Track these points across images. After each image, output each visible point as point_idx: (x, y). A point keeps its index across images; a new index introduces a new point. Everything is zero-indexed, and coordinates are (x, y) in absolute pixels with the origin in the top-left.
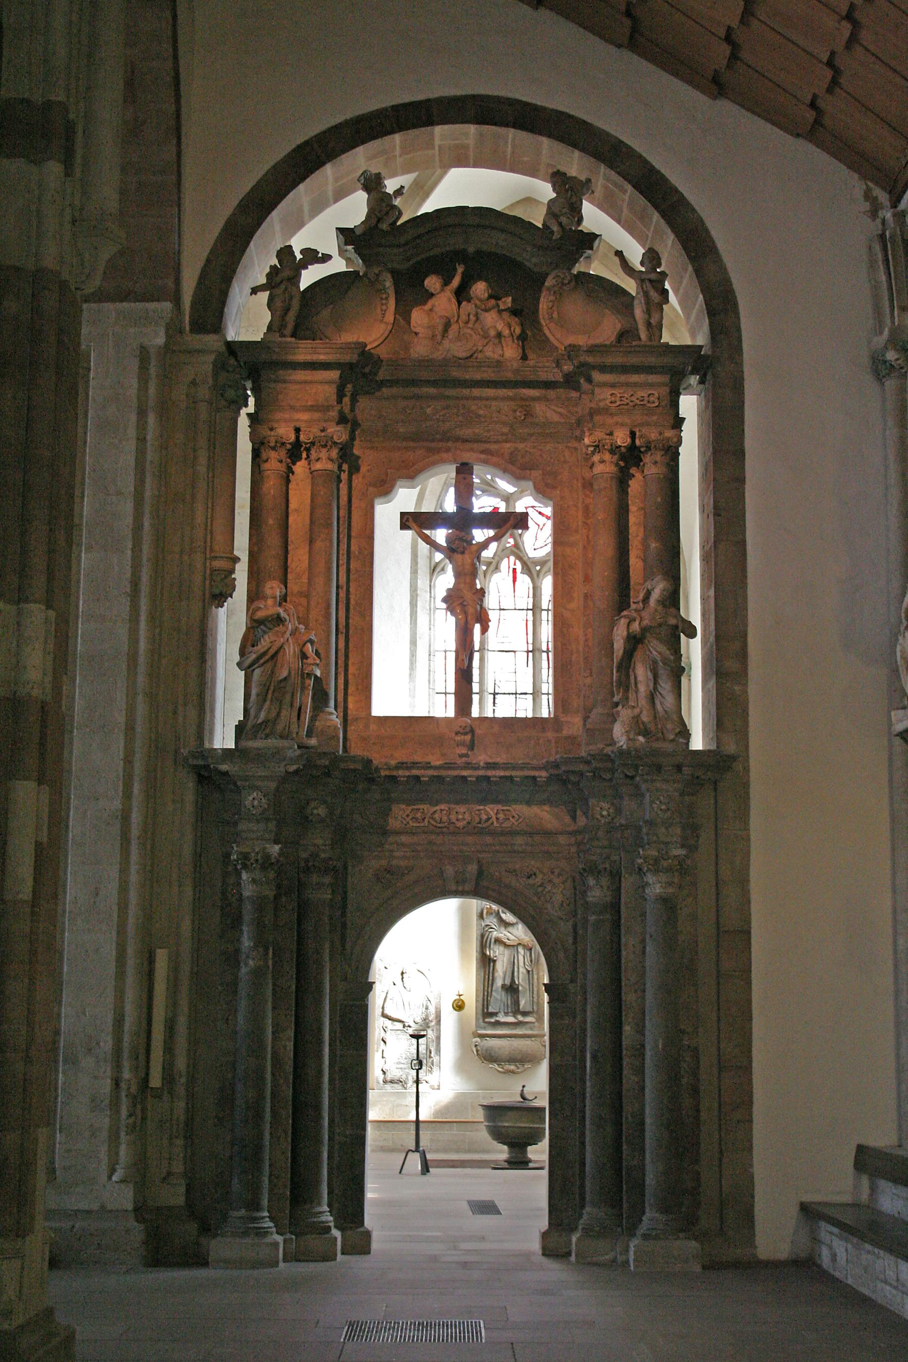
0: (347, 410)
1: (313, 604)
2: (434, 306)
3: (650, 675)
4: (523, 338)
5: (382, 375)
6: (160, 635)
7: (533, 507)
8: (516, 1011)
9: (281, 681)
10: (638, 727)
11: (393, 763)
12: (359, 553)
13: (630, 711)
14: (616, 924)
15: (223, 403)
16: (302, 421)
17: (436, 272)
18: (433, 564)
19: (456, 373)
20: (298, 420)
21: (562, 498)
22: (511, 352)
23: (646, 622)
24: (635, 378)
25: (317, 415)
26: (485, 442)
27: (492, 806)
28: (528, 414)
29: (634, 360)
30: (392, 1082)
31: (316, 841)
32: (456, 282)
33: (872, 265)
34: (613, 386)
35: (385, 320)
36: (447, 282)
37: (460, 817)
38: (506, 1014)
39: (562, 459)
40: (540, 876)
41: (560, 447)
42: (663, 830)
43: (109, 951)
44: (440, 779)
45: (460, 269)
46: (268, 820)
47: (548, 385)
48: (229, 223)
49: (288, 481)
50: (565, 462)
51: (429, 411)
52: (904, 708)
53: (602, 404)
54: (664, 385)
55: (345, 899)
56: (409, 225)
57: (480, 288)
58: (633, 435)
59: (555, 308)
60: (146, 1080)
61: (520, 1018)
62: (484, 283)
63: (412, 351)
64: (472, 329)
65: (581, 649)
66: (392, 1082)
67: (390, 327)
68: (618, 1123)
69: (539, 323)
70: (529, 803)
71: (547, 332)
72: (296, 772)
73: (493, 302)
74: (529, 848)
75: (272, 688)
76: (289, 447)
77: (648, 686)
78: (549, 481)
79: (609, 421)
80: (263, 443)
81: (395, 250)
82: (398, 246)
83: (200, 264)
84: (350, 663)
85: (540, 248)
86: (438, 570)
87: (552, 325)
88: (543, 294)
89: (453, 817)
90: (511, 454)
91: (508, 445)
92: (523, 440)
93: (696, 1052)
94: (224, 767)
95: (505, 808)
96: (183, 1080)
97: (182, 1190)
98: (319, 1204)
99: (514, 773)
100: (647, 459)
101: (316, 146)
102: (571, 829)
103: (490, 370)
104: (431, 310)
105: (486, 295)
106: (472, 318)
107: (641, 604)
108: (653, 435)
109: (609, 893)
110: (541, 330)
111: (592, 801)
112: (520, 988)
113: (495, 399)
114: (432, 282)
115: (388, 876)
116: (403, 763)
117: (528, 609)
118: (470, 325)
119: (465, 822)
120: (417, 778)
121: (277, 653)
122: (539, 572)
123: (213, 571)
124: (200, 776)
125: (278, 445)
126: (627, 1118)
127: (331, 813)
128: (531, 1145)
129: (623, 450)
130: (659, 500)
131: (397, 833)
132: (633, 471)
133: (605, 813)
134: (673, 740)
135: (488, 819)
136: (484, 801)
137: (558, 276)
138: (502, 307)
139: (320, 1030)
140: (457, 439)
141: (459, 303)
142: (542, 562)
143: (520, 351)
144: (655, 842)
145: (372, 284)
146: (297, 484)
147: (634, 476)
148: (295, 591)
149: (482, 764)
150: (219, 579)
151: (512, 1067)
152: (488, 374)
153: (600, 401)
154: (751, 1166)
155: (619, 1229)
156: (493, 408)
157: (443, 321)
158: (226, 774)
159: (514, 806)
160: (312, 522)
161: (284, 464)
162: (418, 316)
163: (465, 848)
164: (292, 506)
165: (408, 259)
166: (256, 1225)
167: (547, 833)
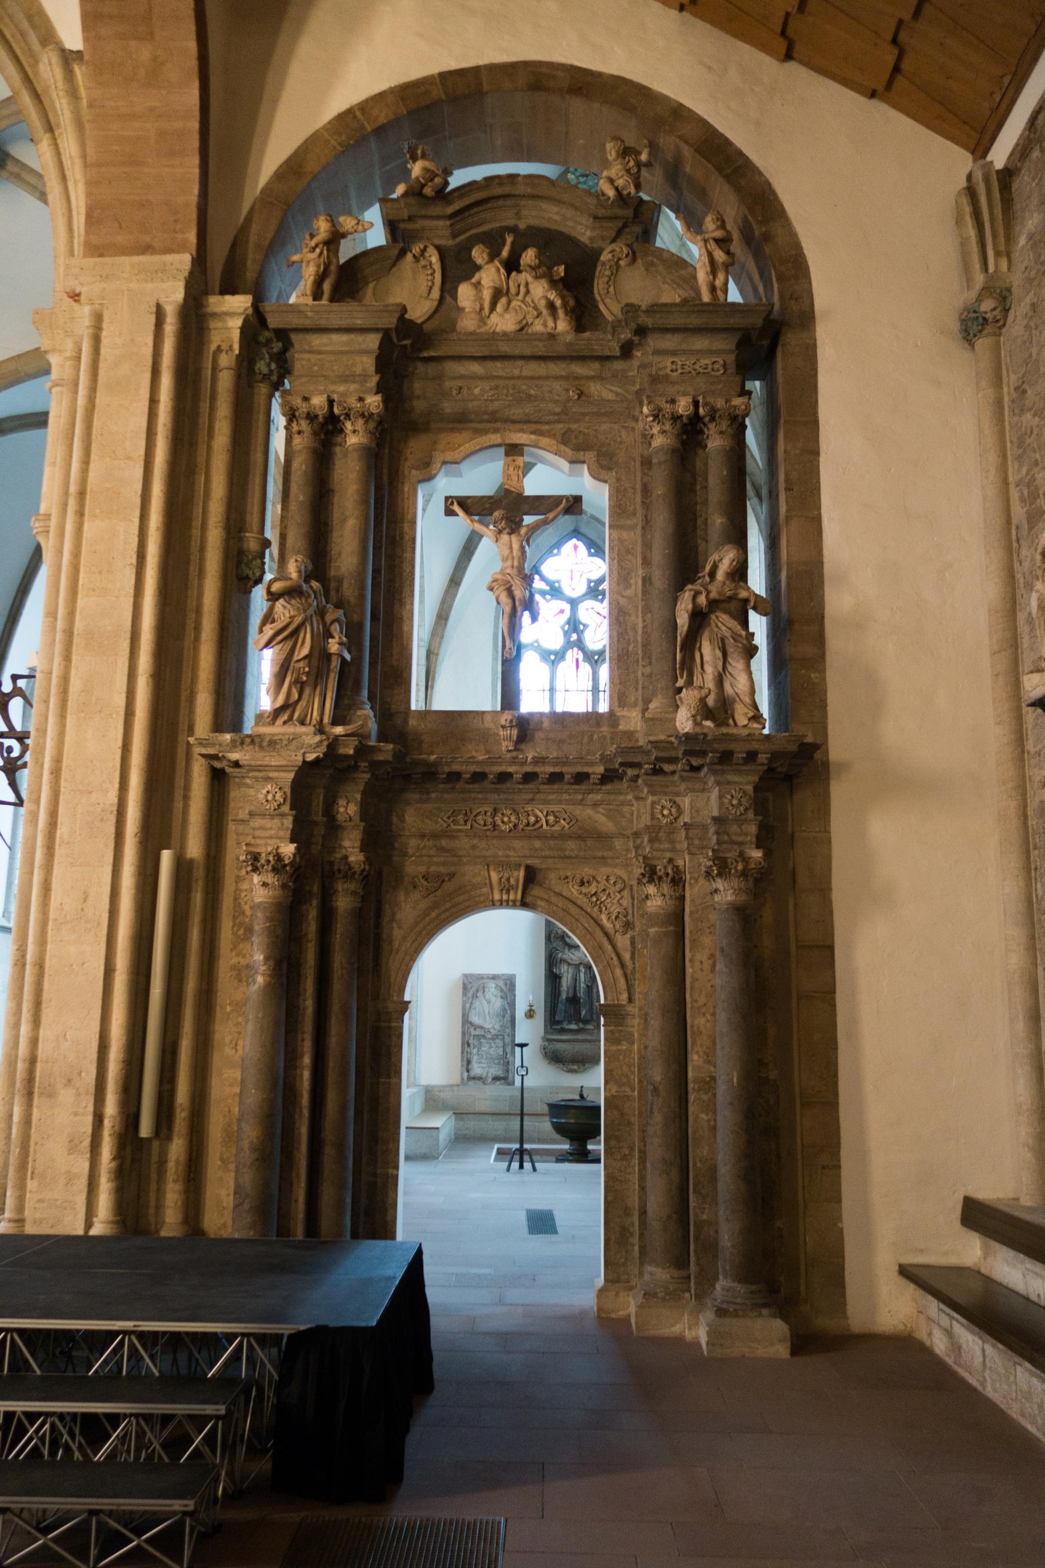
3: (719, 654)
8: (579, 1020)
10: (705, 711)
13: (696, 692)
14: (680, 935)
21: (618, 480)
22: (563, 325)
23: (713, 595)
26: (536, 422)
27: (541, 807)
30: (474, 1078)
33: (959, 222)
34: (674, 353)
36: (494, 255)
39: (619, 439)
40: (594, 884)
41: (616, 427)
46: (282, 815)
51: (477, 391)
52: (1039, 671)
53: (662, 373)
54: (730, 351)
58: (696, 404)
59: (611, 283)
61: (581, 1025)
65: (639, 639)
66: (474, 1078)
68: (684, 1170)
77: (716, 667)
78: (604, 463)
79: (671, 390)
90: (564, 434)
91: (561, 426)
92: (577, 421)
106: (523, 290)
122: (596, 662)
126: (695, 1164)
129: (685, 420)
133: (666, 812)
134: (745, 726)
135: (537, 822)
140: (507, 420)
141: (509, 274)
142: (601, 653)
151: (575, 1067)
152: (540, 348)
153: (661, 369)
154: (840, 1218)
155: (687, 1295)
162: (465, 292)
163: (511, 853)
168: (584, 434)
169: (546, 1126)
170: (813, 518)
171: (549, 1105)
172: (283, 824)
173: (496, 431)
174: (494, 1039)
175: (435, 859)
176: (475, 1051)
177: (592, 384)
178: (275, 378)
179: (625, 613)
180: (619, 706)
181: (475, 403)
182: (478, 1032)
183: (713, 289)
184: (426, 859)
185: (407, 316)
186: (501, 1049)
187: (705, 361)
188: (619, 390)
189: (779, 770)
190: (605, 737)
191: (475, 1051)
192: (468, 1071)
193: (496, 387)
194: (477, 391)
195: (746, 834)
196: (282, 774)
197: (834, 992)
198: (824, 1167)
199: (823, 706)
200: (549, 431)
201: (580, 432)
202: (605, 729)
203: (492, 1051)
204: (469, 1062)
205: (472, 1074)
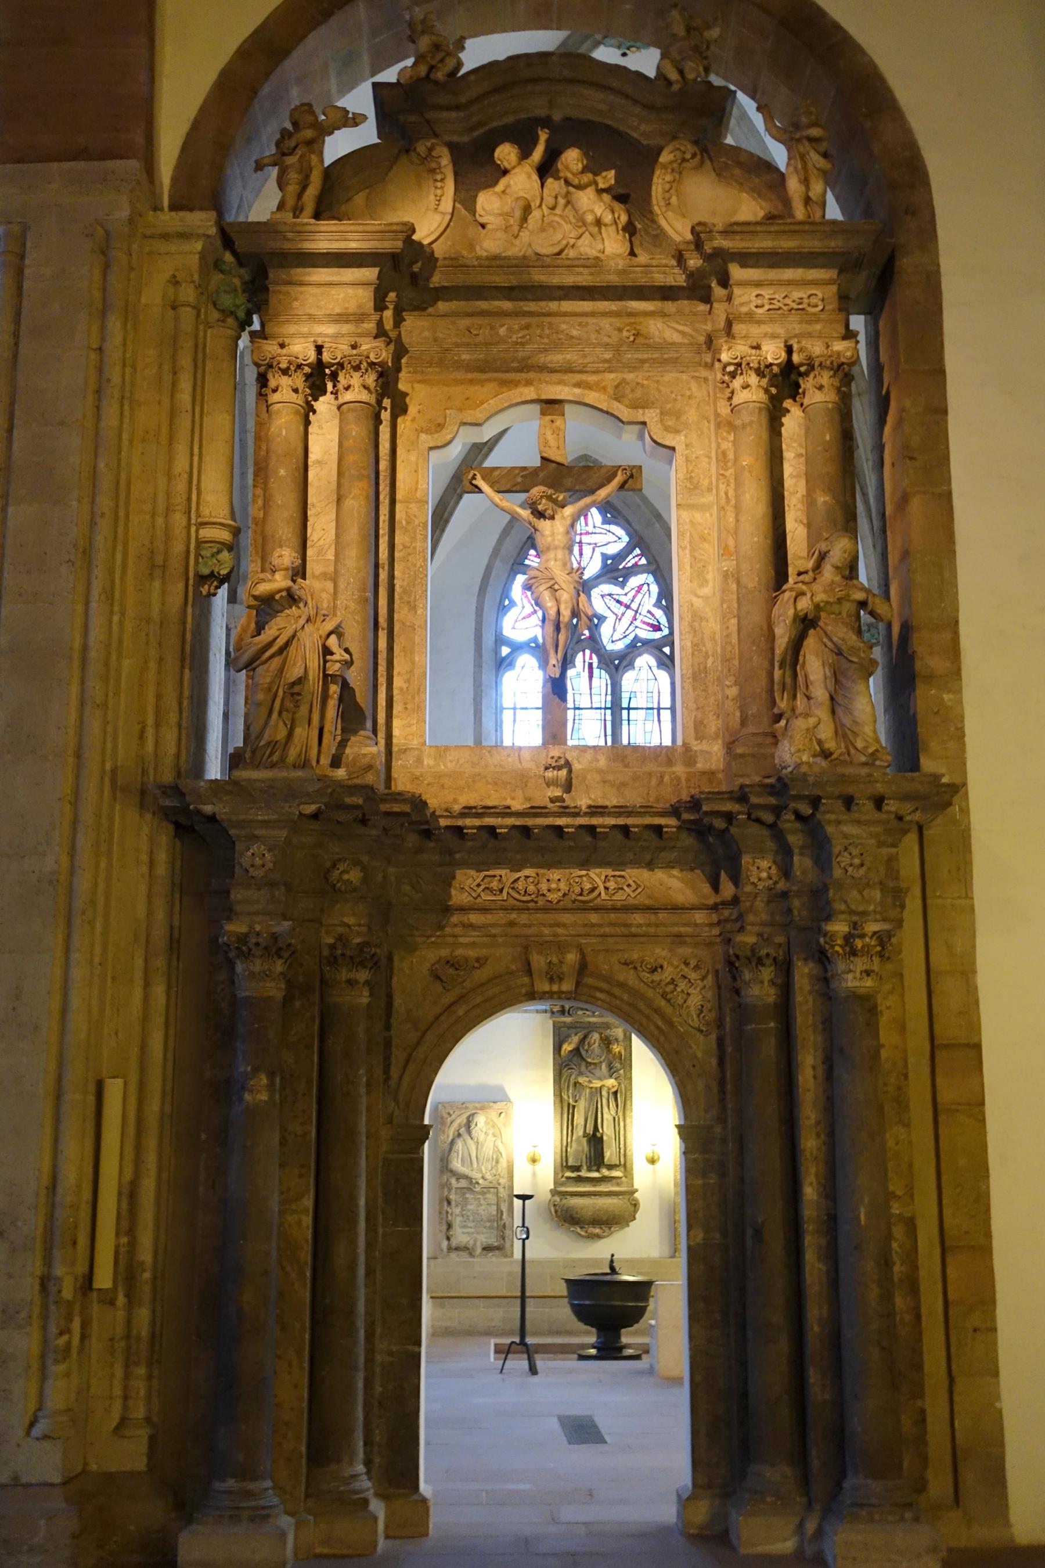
0: (389, 325)
1: (342, 585)
2: (508, 186)
4: (630, 229)
5: (437, 280)
6: (121, 623)
7: (610, 595)
9: (293, 684)
11: (457, 808)
12: (408, 523)
15: (215, 315)
16: (326, 336)
17: (513, 141)
18: (499, 660)
19: (539, 277)
20: (320, 335)
22: (612, 245)
23: (821, 597)
24: (789, 274)
25: (346, 328)
26: (580, 372)
27: (598, 870)
29: (787, 244)
30: (457, 1249)
31: (346, 920)
34: (759, 284)
35: (441, 208)
36: (525, 154)
37: (554, 886)
38: (589, 1170)
39: (688, 393)
40: (670, 969)
41: (684, 377)
42: (855, 893)
44: (525, 830)
45: (543, 136)
47: (667, 293)
49: (307, 423)
51: (502, 331)
53: (744, 309)
55: (389, 1006)
56: (472, 77)
57: (572, 158)
58: (789, 350)
59: (673, 191)
60: (89, 1277)
62: (577, 150)
63: (478, 248)
64: (561, 216)
66: (457, 1249)
67: (448, 217)
69: (651, 212)
70: (650, 865)
71: (663, 223)
72: (315, 816)
73: (588, 177)
74: (652, 930)
75: (281, 693)
76: (307, 370)
78: (670, 423)
79: (756, 331)
80: (270, 366)
81: (454, 114)
82: (457, 108)
83: (184, 128)
84: (395, 673)
86: (505, 664)
87: (670, 214)
88: (658, 172)
89: (544, 887)
90: (617, 387)
91: (612, 376)
92: (633, 369)
93: (911, 1225)
94: (208, 809)
95: (617, 873)
96: (147, 1275)
97: (143, 1447)
98: (351, 1462)
99: (630, 821)
100: (807, 384)
102: (710, 902)
103: (586, 271)
104: (504, 192)
105: (580, 166)
106: (562, 201)
107: (811, 573)
108: (817, 349)
109: (772, 991)
110: (653, 221)
111: (746, 859)
112: (605, 1138)
113: (593, 314)
114: (506, 153)
115: (449, 971)
116: (470, 808)
117: (606, 708)
118: (558, 211)
119: (560, 894)
120: (491, 830)
121: (287, 644)
122: (617, 668)
123: (199, 543)
124: (177, 825)
125: (292, 368)
127: (365, 880)
128: (625, 1327)
129: (776, 369)
130: (828, 437)
131: (463, 909)
132: (788, 403)
136: (585, 864)
137: (679, 149)
138: (601, 186)
139: (353, 1198)
140: (542, 369)
143: (628, 244)
144: (843, 913)
145: (424, 160)
146: (321, 427)
147: (788, 411)
148: (317, 573)
149: (584, 808)
150: (209, 555)
151: (597, 1231)
152: (584, 278)
154: (998, 1398)
157: (521, 203)
158: (212, 818)
159: (629, 871)
160: (340, 474)
161: (301, 396)
162: (487, 203)
163: (560, 931)
164: (312, 457)
165: (472, 129)
166: (253, 1504)
167: (675, 908)
168: (643, 386)
169: (564, 1312)
170: (940, 495)
171: (568, 1281)
172: (273, 896)
173: (529, 383)
174: (483, 1193)
175: (462, 940)
176: (458, 1211)
177: (652, 322)
178: (241, 314)
179: (701, 619)
180: (696, 739)
181: (501, 347)
182: (463, 1183)
183: (807, 200)
184: (450, 940)
185: (414, 237)
186: (495, 1207)
187: (797, 294)
188: (687, 329)
189: (908, 818)
190: (678, 779)
191: (458, 1211)
192: (448, 1239)
193: (527, 327)
194: (502, 331)
195: (868, 902)
196: (275, 833)
197: (983, 1104)
198: (975, 1330)
199: (960, 735)
200: (597, 383)
201: (638, 384)
202: (679, 769)
203: (481, 1211)
204: (449, 1226)
205: (454, 1243)
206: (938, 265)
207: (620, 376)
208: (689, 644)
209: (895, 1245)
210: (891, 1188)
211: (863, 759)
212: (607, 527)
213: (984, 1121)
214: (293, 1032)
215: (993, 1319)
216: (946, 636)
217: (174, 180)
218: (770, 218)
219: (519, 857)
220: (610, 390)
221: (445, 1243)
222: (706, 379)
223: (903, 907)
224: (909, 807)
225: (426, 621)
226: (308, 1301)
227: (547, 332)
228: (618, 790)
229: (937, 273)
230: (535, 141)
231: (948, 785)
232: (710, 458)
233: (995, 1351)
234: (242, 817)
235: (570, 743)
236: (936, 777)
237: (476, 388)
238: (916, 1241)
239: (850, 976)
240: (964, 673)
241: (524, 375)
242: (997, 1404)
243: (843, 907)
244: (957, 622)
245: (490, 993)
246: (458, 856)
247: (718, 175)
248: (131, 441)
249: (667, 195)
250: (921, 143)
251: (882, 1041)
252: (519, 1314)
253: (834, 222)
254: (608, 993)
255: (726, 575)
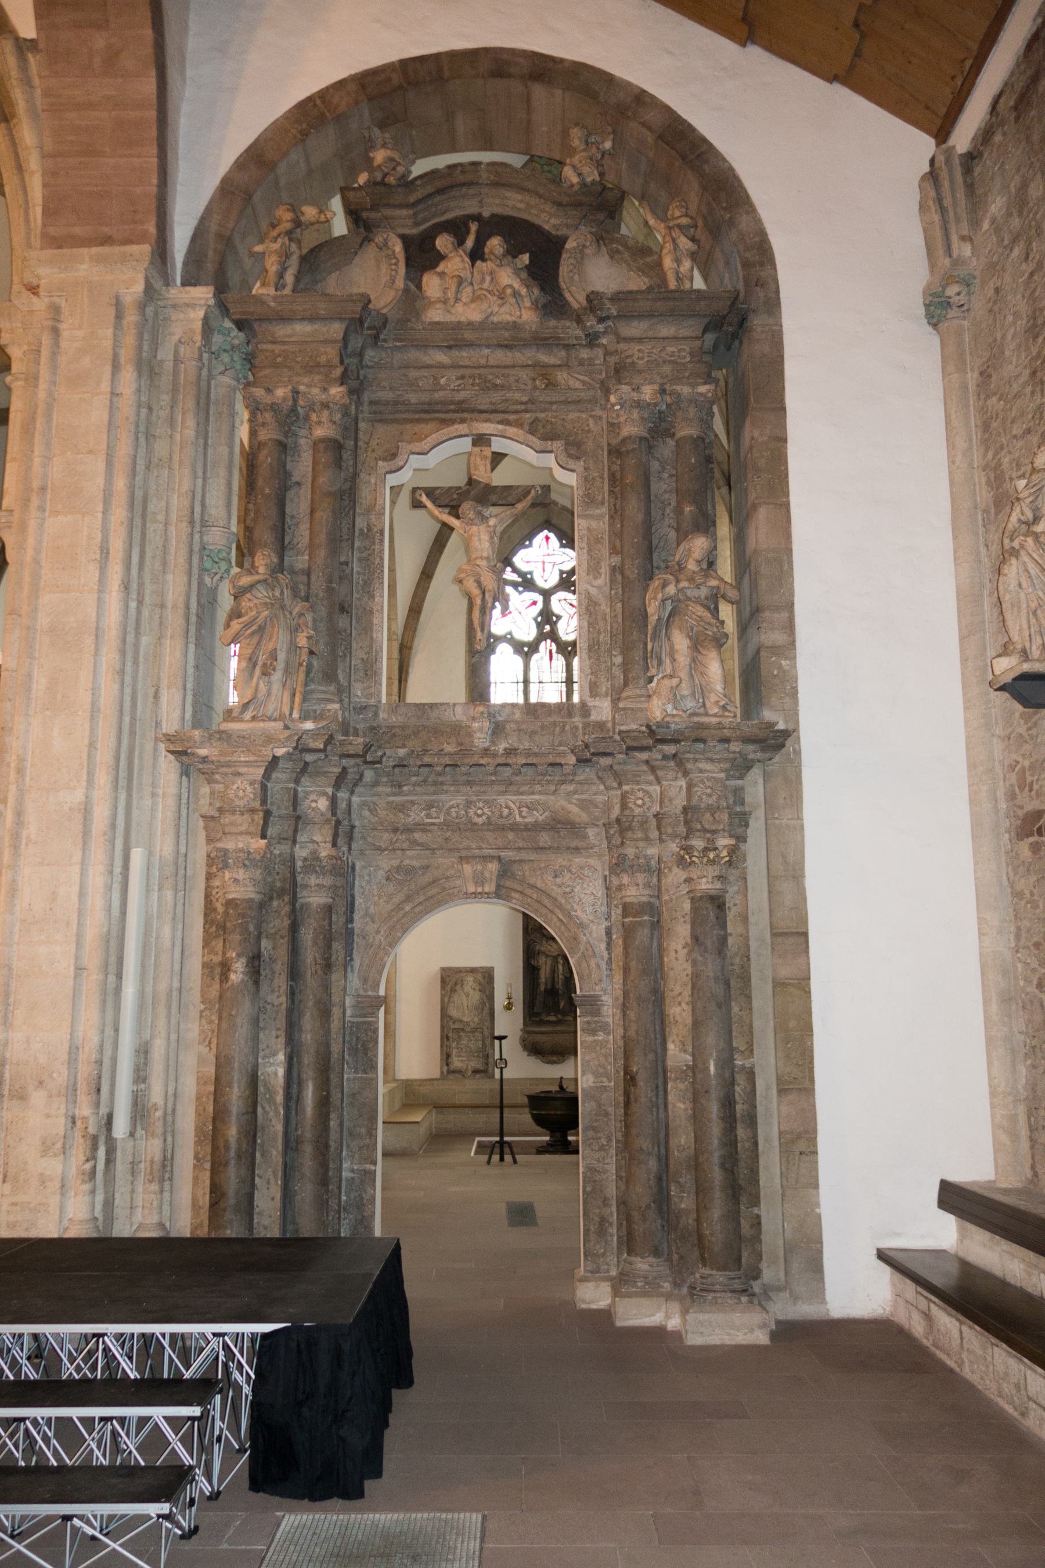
28: (551, 385)
30: (454, 1072)
32: (470, 243)
39: (587, 428)
42: (708, 815)
43: (66, 966)
45: (474, 227)
48: (225, 181)
50: (588, 431)
51: (443, 381)
57: (495, 244)
64: (487, 290)
66: (454, 1072)
69: (558, 286)
81: (404, 212)
82: (407, 206)
85: (560, 205)
91: (528, 415)
92: (544, 411)
101: (318, 102)
110: (562, 295)
114: (443, 242)
144: (699, 831)
151: (555, 1058)
153: (627, 357)
154: (818, 1205)
156: (512, 379)
168: (551, 423)
172: (253, 820)
173: (463, 421)
176: (454, 1045)
177: (559, 373)
180: (591, 696)
188: (586, 379)
192: (447, 1065)
193: (462, 377)
194: (443, 381)
195: (719, 822)
197: (809, 979)
199: (794, 693)
205: (452, 1067)
206: (781, 326)
207: (534, 415)
208: (586, 624)
209: (737, 1089)
210: (735, 1044)
211: (716, 710)
212: (563, 550)
213: (809, 992)
214: (271, 925)
215: (815, 1146)
216: (785, 615)
217: (185, 264)
218: (650, 289)
219: (452, 788)
220: (527, 427)
221: (445, 1068)
222: (600, 418)
223: (747, 825)
224: (751, 747)
225: (382, 606)
226: (280, 1134)
227: (477, 381)
228: (530, 736)
229: (780, 333)
230: (468, 232)
231: (782, 731)
232: (603, 478)
233: (816, 1170)
234: (228, 759)
235: (493, 701)
236: (771, 725)
237: (422, 425)
238: (755, 1085)
239: (704, 880)
240: (798, 644)
241: (460, 415)
242: (817, 1210)
243: (699, 827)
244: (793, 604)
245: (430, 894)
246: (405, 788)
247: (612, 257)
248: (148, 468)
249: (571, 275)
250: (769, 231)
251: (729, 931)
252: (498, 1120)
253: (698, 291)
254: (521, 893)
255: (613, 569)
